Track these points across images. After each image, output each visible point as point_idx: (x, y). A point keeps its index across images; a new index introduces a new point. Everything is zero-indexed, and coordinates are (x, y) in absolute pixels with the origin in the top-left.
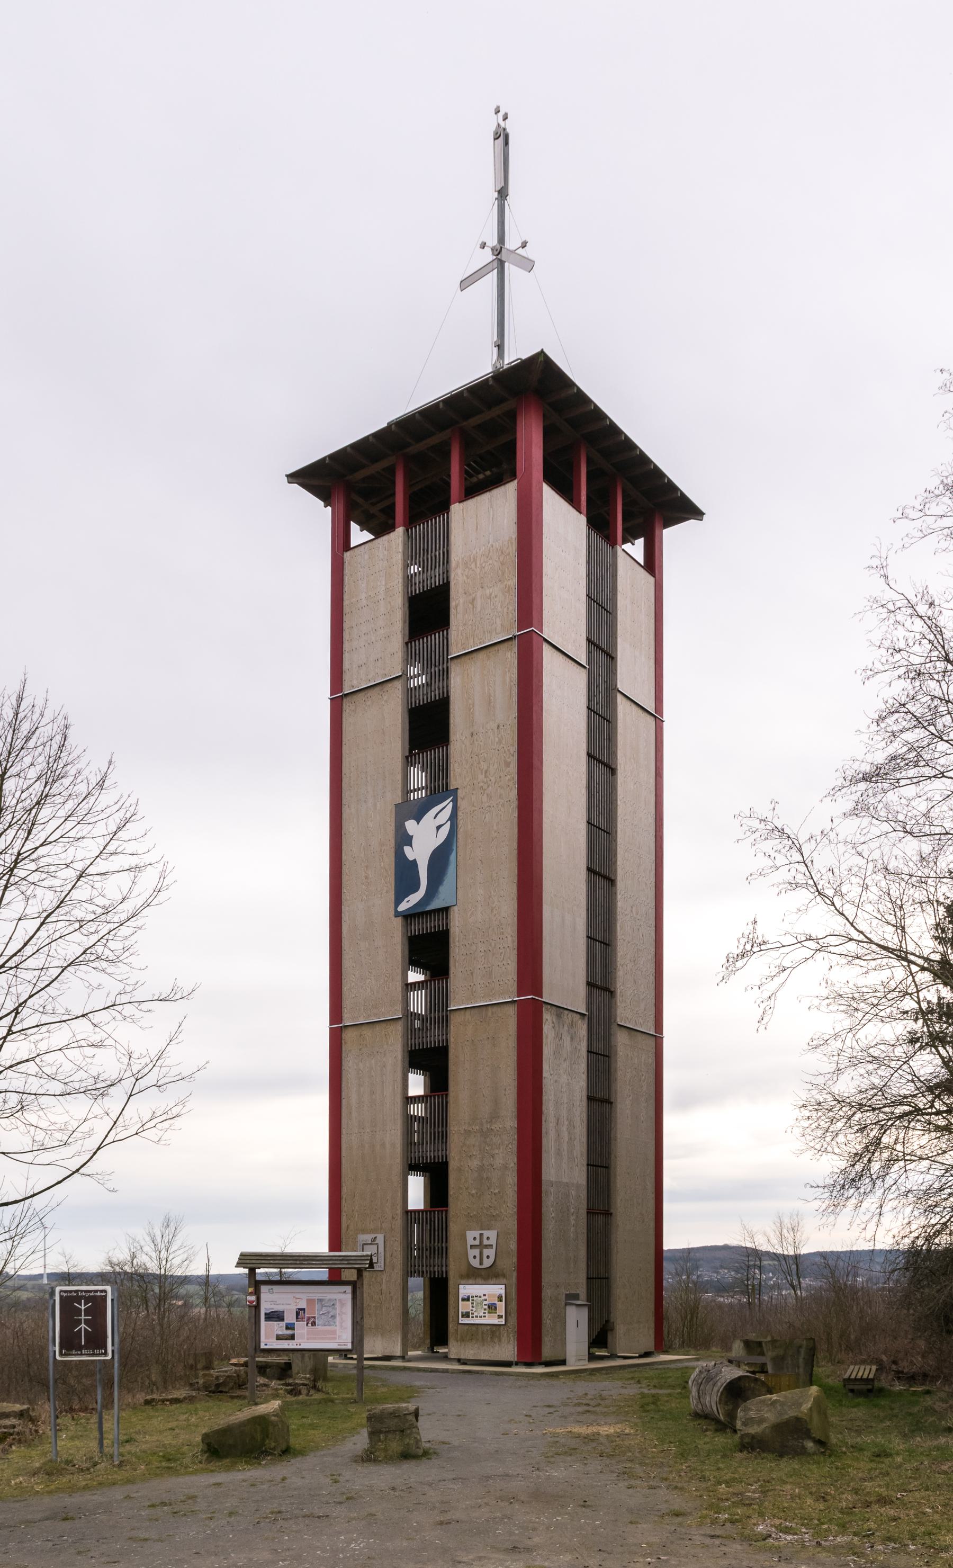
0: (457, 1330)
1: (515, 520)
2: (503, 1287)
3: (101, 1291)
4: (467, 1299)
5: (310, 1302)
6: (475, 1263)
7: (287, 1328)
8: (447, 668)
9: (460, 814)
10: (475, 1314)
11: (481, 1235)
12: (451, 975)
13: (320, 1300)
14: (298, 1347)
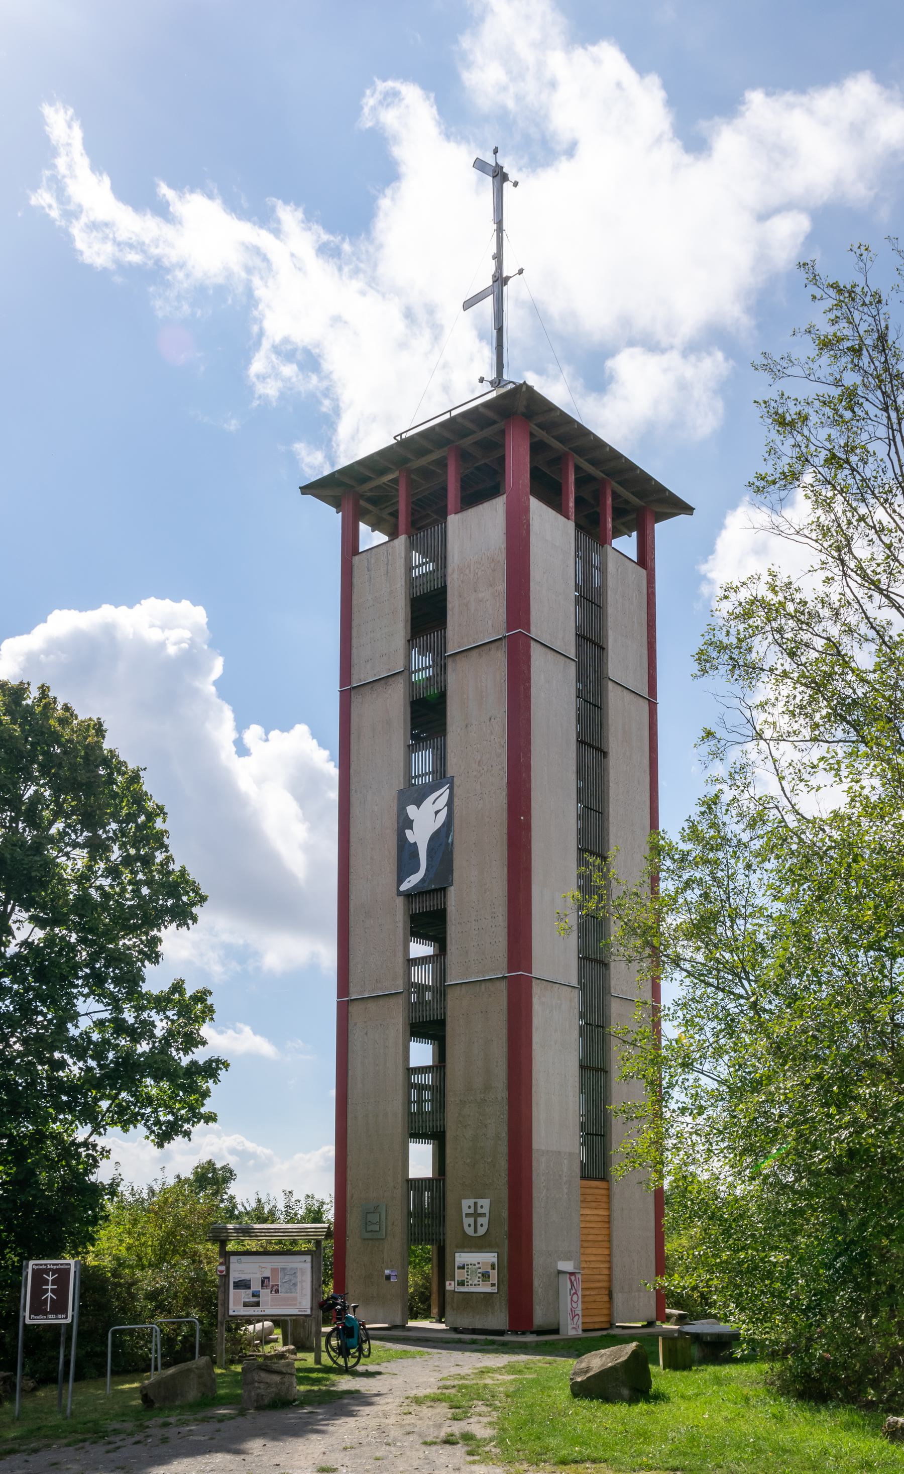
0: (453, 1298)
1: (504, 531)
2: (496, 1255)
3: (66, 1264)
4: (462, 1267)
5: (274, 1270)
6: (470, 1231)
7: (253, 1296)
8: (445, 664)
9: (456, 800)
10: (470, 1282)
11: (476, 1204)
12: (448, 952)
13: (283, 1269)
14: (263, 1313)
